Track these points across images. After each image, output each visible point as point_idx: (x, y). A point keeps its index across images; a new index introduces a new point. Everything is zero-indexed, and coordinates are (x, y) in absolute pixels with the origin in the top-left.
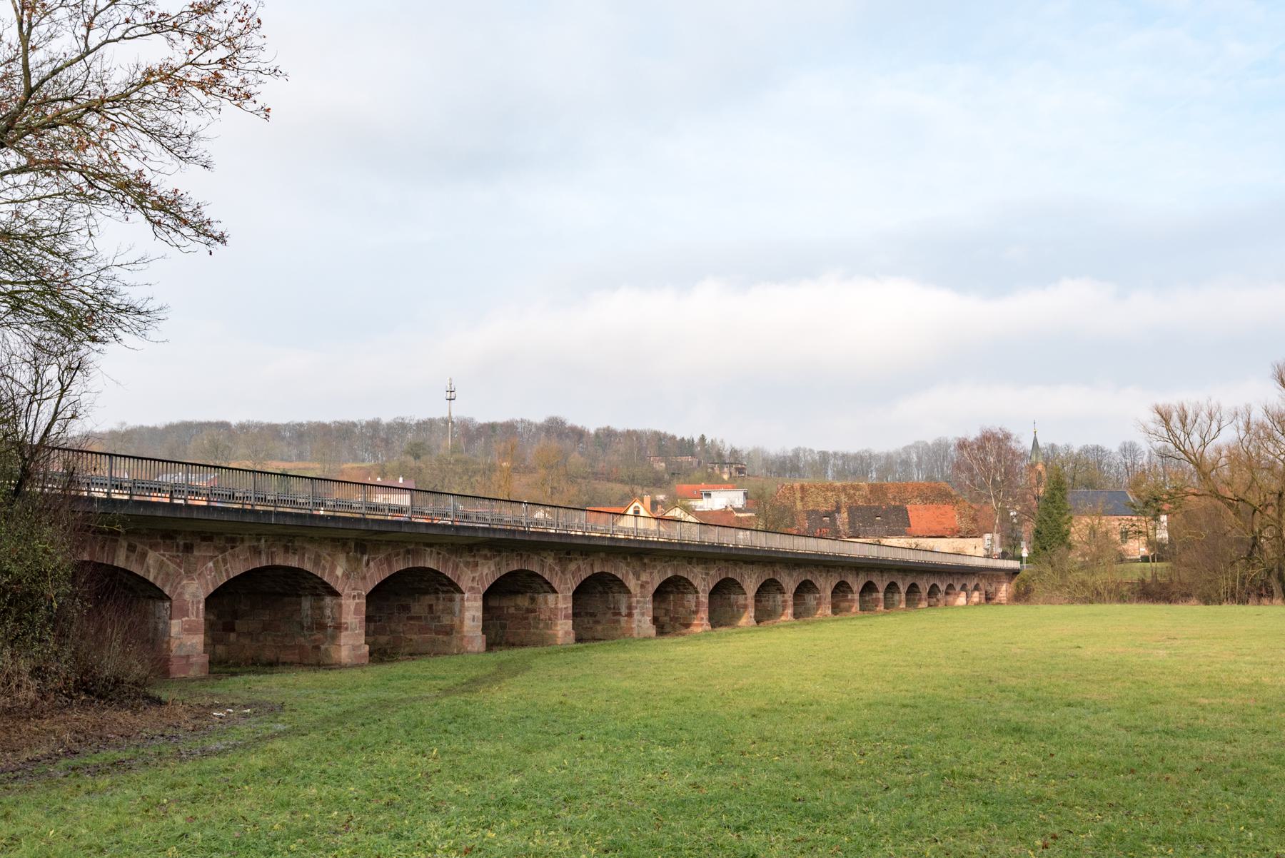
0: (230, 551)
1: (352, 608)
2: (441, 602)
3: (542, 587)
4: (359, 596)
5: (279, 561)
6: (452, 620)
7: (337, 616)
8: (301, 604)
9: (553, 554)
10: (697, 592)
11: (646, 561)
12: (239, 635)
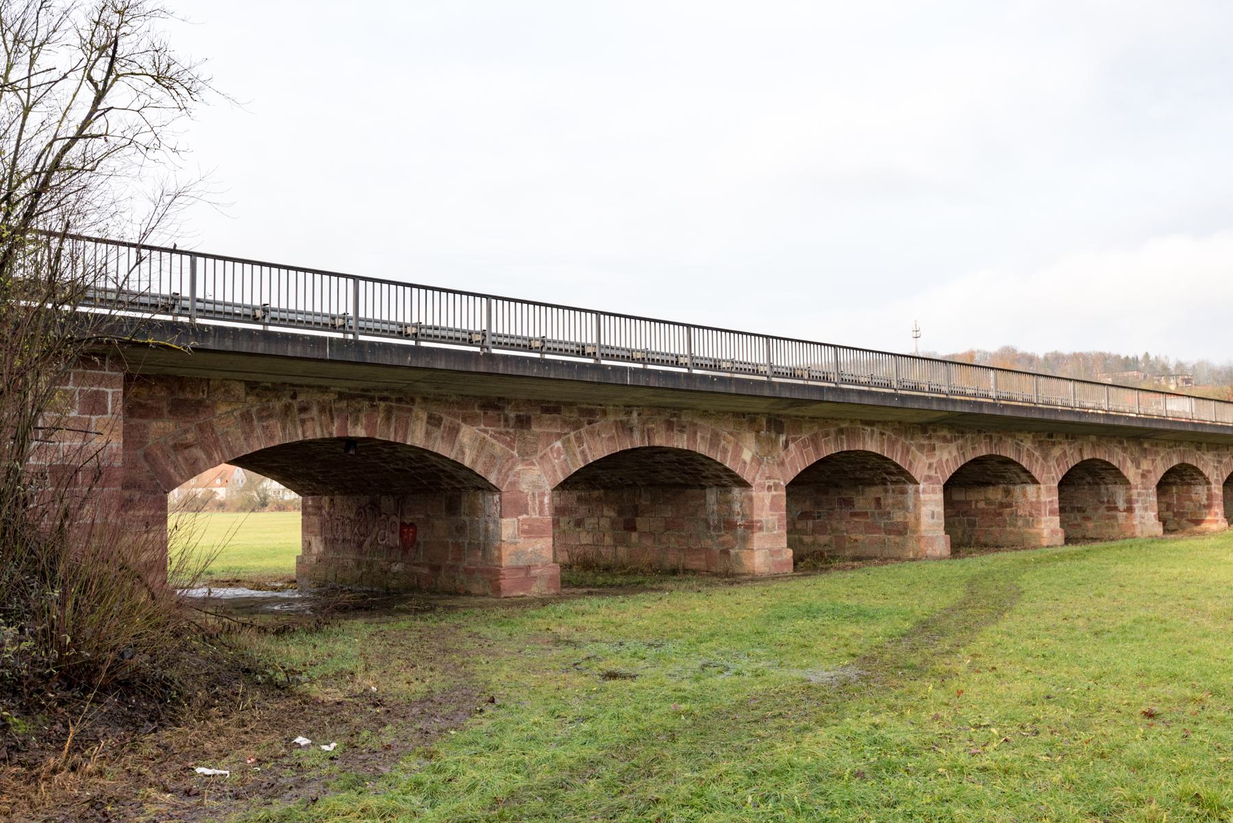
0: (587, 426)
1: (767, 502)
2: (890, 494)
3: (1018, 476)
4: (776, 486)
5: (659, 441)
6: (906, 518)
7: (748, 512)
8: (705, 497)
9: (1030, 436)
10: (1208, 483)
11: (1146, 446)
12: (642, 534)
